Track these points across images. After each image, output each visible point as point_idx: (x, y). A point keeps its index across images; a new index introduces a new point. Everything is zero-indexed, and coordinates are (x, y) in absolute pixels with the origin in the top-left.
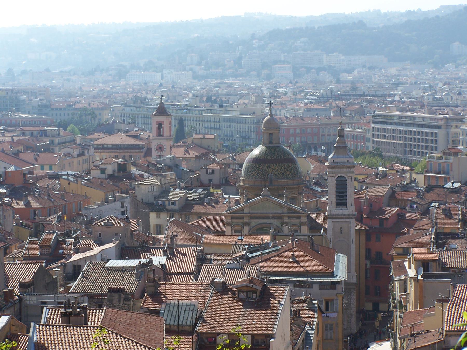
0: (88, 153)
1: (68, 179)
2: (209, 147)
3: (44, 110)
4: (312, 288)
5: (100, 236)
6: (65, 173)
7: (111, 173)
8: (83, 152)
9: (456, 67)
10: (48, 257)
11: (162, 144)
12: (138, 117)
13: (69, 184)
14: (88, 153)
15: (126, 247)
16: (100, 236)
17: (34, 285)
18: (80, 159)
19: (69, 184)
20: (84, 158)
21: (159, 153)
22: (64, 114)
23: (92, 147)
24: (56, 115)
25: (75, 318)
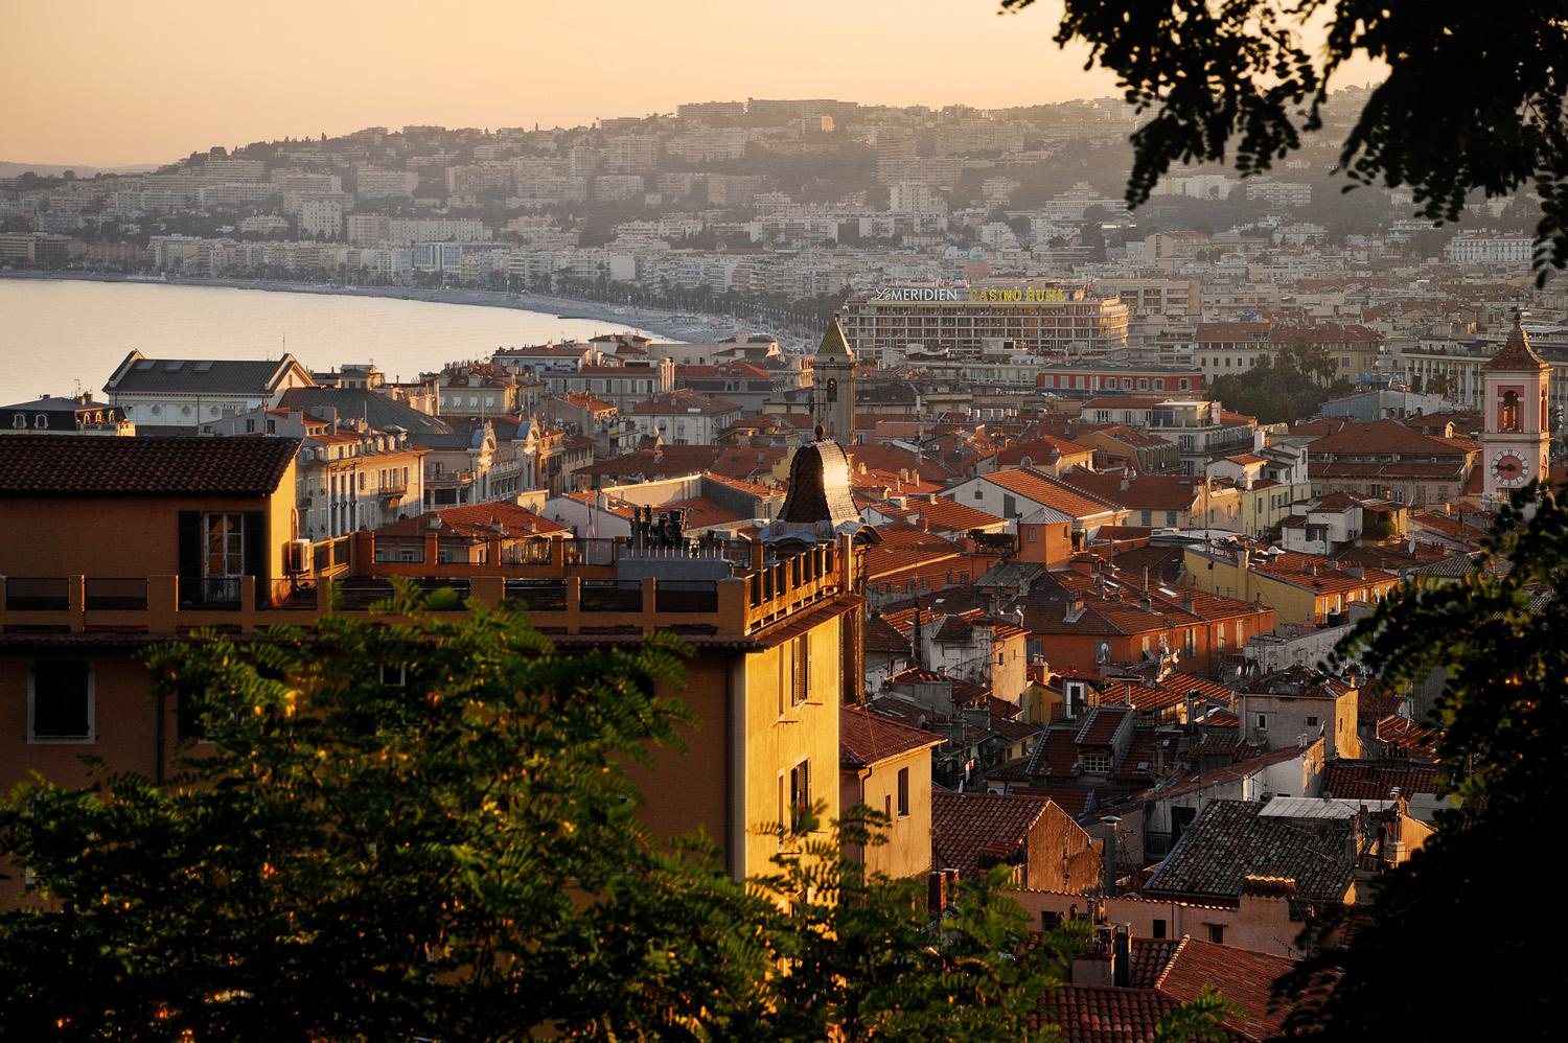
0: (1288, 476)
1: (1206, 554)
2: (250, 424)
3: (1178, 347)
4: (1292, 919)
5: (1262, 724)
6: (1200, 535)
7: (1342, 538)
8: (1273, 475)
9: (1155, 150)
10: (1104, 780)
11: (1514, 454)
12: (1463, 372)
13: (1211, 567)
14: (1288, 476)
15: (1341, 760)
16: (1262, 724)
17: (1025, 861)
18: (1263, 494)
19: (1211, 567)
20: (1275, 491)
21: (1506, 482)
22: (1216, 361)
23: (1300, 460)
24: (1216, 362)
25: (1088, 963)
